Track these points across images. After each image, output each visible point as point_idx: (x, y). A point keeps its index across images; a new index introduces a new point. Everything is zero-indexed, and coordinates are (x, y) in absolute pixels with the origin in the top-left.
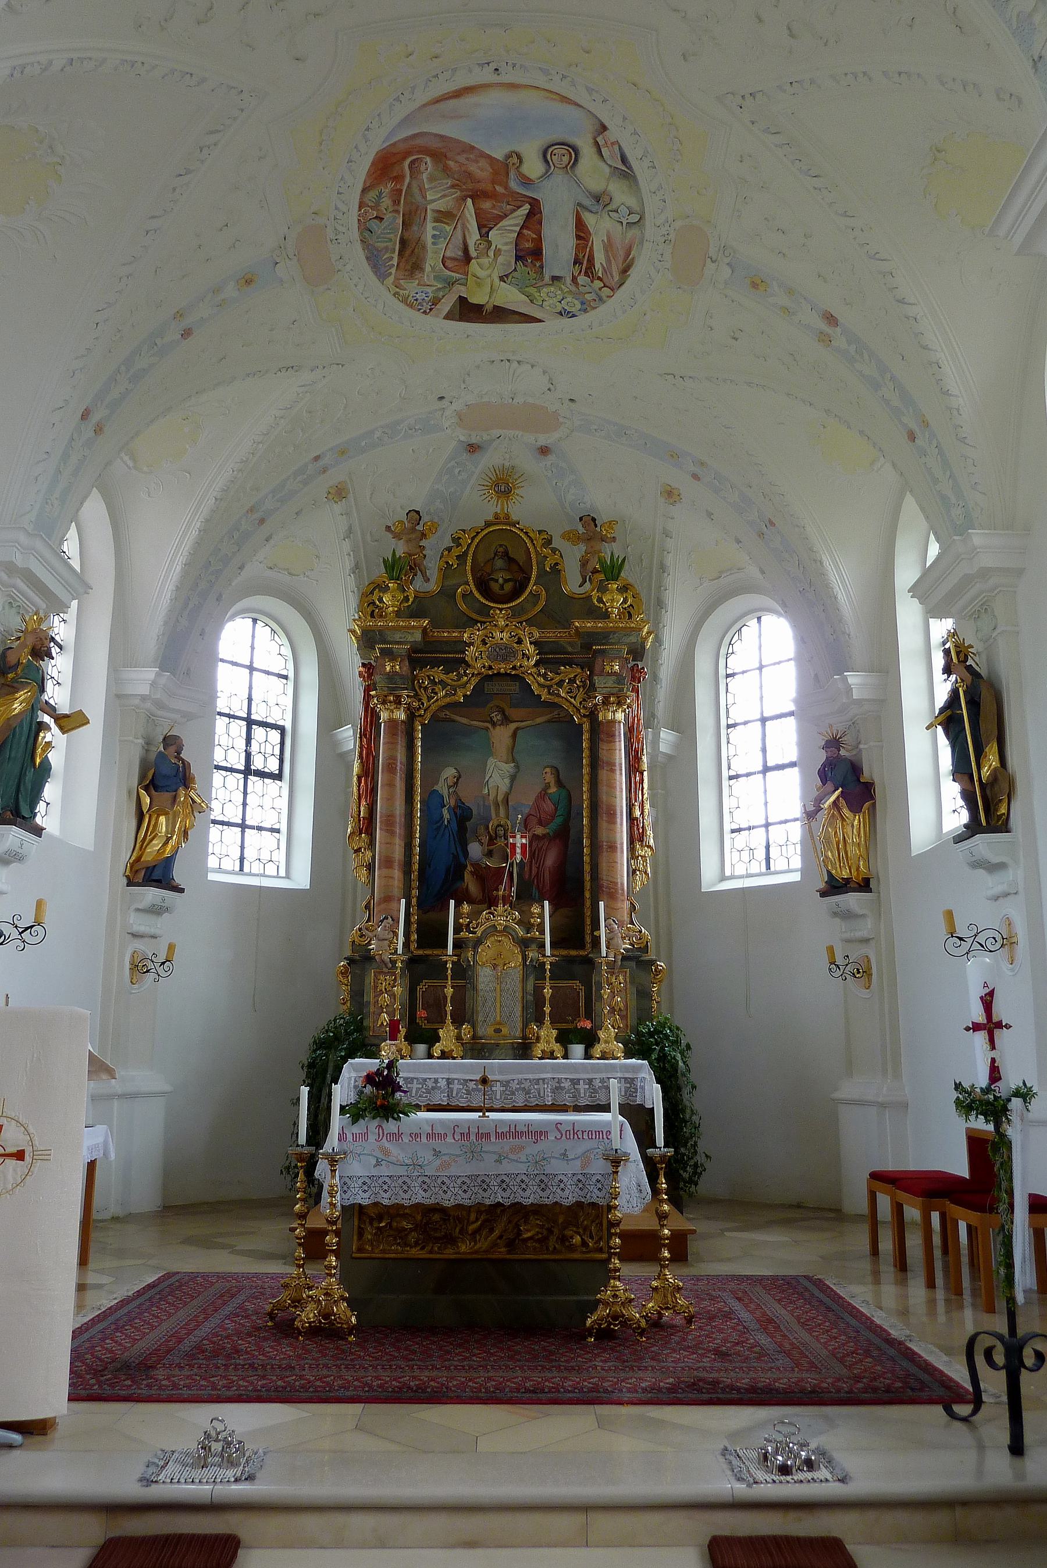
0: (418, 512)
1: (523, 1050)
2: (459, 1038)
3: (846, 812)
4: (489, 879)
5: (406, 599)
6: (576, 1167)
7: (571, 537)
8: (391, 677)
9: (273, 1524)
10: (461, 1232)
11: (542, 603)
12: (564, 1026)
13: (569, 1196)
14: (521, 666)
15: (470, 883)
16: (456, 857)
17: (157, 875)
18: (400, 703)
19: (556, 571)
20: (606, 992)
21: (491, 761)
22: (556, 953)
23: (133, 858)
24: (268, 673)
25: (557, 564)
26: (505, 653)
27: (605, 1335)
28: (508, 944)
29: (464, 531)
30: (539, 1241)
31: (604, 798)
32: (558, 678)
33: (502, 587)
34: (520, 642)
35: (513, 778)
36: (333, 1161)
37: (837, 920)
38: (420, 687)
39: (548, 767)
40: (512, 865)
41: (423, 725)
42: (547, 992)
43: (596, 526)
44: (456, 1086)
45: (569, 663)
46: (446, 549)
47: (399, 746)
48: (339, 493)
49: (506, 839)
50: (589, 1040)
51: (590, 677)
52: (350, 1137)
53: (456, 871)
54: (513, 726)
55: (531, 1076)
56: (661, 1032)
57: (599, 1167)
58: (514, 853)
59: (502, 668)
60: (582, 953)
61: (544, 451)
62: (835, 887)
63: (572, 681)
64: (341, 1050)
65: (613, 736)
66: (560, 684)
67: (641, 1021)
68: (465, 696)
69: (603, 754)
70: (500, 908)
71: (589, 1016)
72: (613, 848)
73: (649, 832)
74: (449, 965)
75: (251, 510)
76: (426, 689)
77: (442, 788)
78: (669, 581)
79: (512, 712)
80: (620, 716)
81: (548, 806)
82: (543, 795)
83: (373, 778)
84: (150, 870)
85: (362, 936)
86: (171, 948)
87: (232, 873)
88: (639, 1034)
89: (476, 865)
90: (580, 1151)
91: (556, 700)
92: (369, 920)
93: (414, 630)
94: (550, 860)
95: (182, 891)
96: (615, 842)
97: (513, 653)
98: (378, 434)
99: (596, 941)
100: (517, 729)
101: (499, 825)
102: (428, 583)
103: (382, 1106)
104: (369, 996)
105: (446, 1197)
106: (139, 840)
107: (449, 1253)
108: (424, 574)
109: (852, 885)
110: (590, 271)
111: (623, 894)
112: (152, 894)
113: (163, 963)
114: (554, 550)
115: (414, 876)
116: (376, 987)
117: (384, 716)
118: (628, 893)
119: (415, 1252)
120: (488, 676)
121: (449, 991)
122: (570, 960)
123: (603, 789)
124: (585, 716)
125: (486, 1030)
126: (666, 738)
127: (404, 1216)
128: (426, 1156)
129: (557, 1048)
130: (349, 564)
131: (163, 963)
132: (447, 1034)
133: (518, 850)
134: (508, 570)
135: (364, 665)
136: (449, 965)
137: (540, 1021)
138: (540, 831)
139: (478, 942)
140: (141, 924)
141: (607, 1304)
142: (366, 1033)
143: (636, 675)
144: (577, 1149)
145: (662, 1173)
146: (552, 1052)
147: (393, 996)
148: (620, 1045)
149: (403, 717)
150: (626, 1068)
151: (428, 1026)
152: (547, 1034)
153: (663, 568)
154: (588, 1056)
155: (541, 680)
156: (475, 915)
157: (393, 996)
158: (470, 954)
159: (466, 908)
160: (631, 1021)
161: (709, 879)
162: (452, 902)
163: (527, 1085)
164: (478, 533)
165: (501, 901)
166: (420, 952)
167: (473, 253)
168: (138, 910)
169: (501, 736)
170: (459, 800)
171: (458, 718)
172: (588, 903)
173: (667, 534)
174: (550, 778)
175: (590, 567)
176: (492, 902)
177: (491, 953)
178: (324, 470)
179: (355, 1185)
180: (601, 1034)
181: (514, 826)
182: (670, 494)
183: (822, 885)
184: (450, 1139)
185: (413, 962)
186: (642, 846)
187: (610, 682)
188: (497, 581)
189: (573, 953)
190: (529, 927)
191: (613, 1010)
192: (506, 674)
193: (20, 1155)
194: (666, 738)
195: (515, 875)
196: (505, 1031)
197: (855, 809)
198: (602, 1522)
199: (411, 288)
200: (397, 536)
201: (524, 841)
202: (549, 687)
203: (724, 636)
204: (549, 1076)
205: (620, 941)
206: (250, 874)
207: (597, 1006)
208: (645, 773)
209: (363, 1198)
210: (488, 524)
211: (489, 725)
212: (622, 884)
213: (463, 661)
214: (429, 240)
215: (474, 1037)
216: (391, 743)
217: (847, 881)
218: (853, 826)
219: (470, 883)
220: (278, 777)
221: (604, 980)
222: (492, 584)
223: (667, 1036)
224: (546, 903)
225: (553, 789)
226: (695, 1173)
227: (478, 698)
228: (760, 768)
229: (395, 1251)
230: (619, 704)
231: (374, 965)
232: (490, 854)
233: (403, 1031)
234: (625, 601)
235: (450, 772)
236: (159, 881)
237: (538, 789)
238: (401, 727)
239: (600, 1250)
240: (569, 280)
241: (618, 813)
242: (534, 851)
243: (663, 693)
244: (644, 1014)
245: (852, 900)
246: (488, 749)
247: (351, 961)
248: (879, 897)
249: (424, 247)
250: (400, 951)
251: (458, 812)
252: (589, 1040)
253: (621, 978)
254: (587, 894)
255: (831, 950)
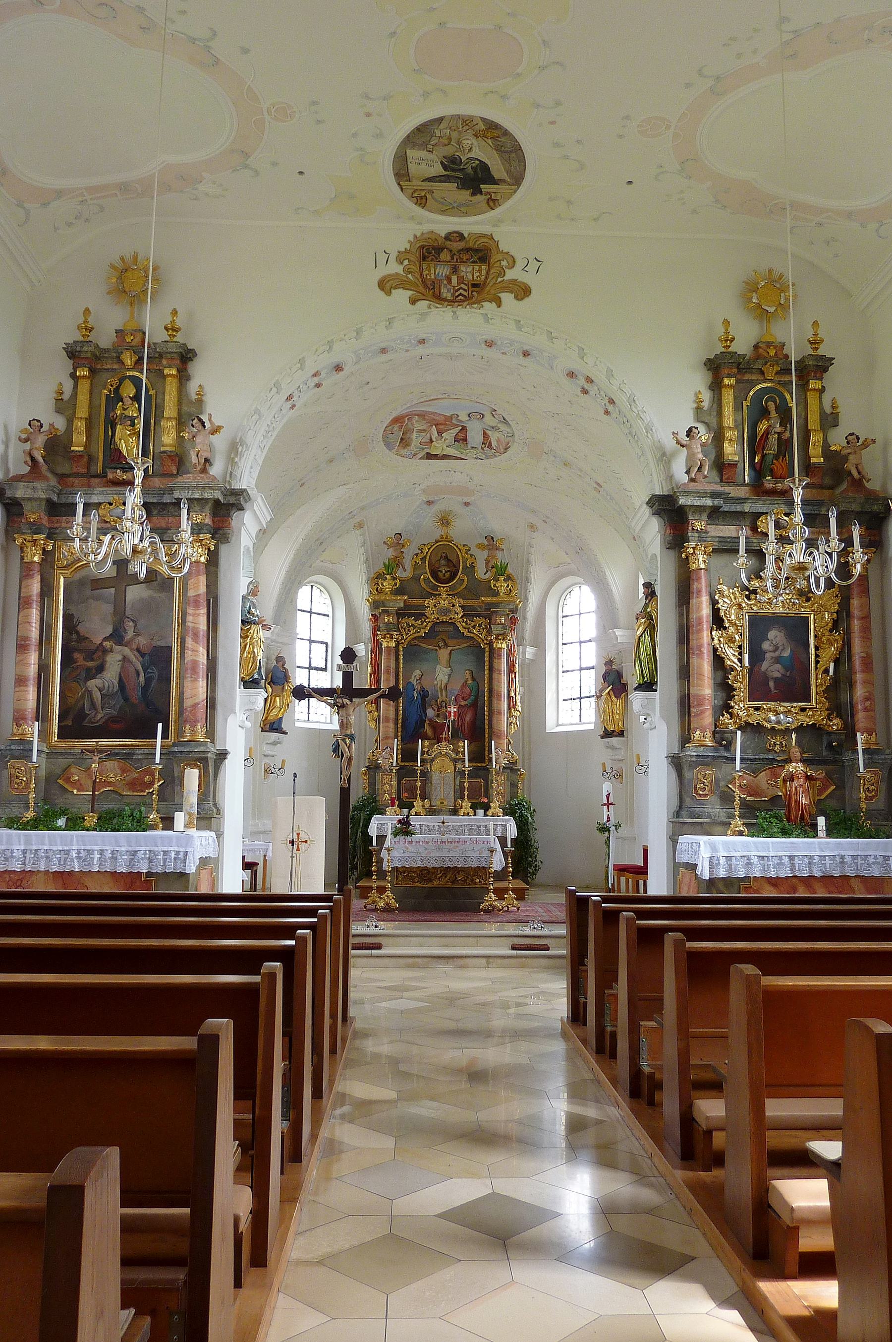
0: (400, 534)
1: (455, 812)
2: (423, 806)
3: (613, 697)
4: (437, 731)
5: (396, 584)
6: (477, 854)
7: (480, 546)
8: (388, 624)
9: (391, 940)
10: (434, 877)
11: (465, 583)
12: (474, 801)
13: (475, 864)
14: (454, 618)
15: (428, 729)
16: (420, 716)
17: (275, 726)
18: (392, 638)
19: (472, 566)
20: (495, 785)
21: (438, 666)
22: (470, 765)
23: (264, 718)
24: (319, 614)
25: (473, 563)
26: (446, 611)
27: (487, 911)
28: (447, 760)
29: (424, 545)
30: (463, 881)
31: (495, 687)
32: (473, 624)
33: (444, 576)
34: (453, 606)
35: (450, 676)
36: (388, 850)
37: (609, 750)
38: (402, 628)
39: (469, 670)
40: (449, 721)
41: (403, 648)
42: (467, 785)
43: (494, 541)
44: (424, 828)
45: (479, 616)
46: (415, 554)
47: (392, 660)
48: (360, 525)
49: (446, 708)
50: (486, 807)
51: (490, 624)
52: (393, 842)
53: (421, 723)
54: (450, 648)
55: (458, 824)
56: (521, 804)
57: (486, 853)
58: (450, 715)
59: (445, 619)
60: (484, 765)
61: (467, 504)
62: (607, 734)
63: (480, 625)
64: (367, 811)
65: (501, 656)
66: (474, 627)
67: (512, 798)
68: (425, 633)
69: (495, 665)
70: (443, 743)
71: (487, 796)
72: (499, 713)
73: (519, 704)
74: (419, 772)
75: (317, 540)
76: (404, 629)
77: (413, 681)
78: (532, 569)
79: (450, 642)
80: (504, 646)
81: (467, 690)
82: (465, 684)
83: (378, 675)
84: (272, 724)
85: (373, 756)
86: (283, 761)
87: (304, 721)
88: (510, 805)
89: (430, 720)
90: (479, 848)
91: (472, 635)
92: (376, 749)
93: (399, 602)
94: (468, 718)
95: (287, 733)
96: (501, 710)
97: (450, 612)
98: (382, 500)
99: (490, 760)
100: (452, 650)
101: (443, 701)
102: (405, 573)
103: (405, 831)
104: (379, 786)
105: (430, 864)
106: (266, 709)
107: (430, 885)
108: (403, 568)
109: (615, 734)
110: (490, 446)
111: (504, 736)
112: (274, 736)
113: (280, 769)
114: (471, 555)
115: (400, 726)
116: (382, 781)
117: (384, 645)
118: (507, 735)
119: (418, 885)
120: (437, 622)
121: (419, 784)
122: (477, 768)
123: (495, 683)
124: (486, 644)
125: (436, 803)
126: (530, 652)
127: (413, 872)
128: (422, 850)
129: (471, 811)
130: (363, 558)
131: (280, 769)
132: (418, 804)
133: (452, 714)
134: (448, 566)
135: (372, 615)
136: (419, 772)
137: (462, 798)
138: (463, 703)
139: (433, 760)
140: (267, 750)
141: (487, 901)
142: (378, 803)
143: (513, 621)
144: (477, 847)
145: (509, 857)
146: (468, 813)
147: (391, 785)
148: (501, 810)
149: (394, 645)
150: (503, 820)
151: (408, 800)
152: (466, 805)
153: (529, 562)
154: (485, 815)
155: (464, 624)
156: (431, 746)
157: (391, 785)
158: (428, 766)
159: (426, 743)
160: (507, 798)
161: (551, 726)
162: (420, 740)
163: (456, 828)
164: (432, 546)
165: (444, 740)
166: (403, 764)
167: (434, 439)
168: (267, 743)
169: (444, 654)
170: (422, 687)
171: (421, 644)
172: (487, 740)
173: (530, 545)
174: (468, 676)
175: (490, 565)
176: (439, 741)
177: (439, 765)
178: (354, 516)
179: (396, 860)
180: (492, 805)
181: (450, 701)
182: (532, 527)
183: (602, 733)
184: (430, 843)
185: (401, 769)
186: (515, 710)
187: (500, 628)
188: (441, 572)
189: (479, 765)
190: (457, 753)
191: (498, 794)
192: (446, 622)
193: (306, 842)
194: (530, 652)
195: (450, 726)
196: (445, 803)
197: (618, 697)
198: (481, 940)
199: (404, 452)
200: (389, 547)
201: (455, 710)
202: (469, 628)
203: (562, 595)
204: (467, 823)
205: (502, 760)
206: (313, 722)
207: (490, 791)
208: (517, 674)
209: (399, 865)
210: (437, 542)
211: (438, 648)
212: (504, 731)
213: (424, 614)
214: (414, 437)
215: (430, 806)
216: (388, 659)
217: (613, 731)
218: (616, 704)
219: (428, 729)
220: (325, 670)
221: (494, 779)
222: (439, 573)
223: (524, 805)
224: (466, 741)
225: (470, 682)
226: (535, 870)
227: (432, 634)
228: (579, 668)
229: (410, 884)
230: (504, 639)
231: (381, 770)
232: (438, 716)
233: (397, 803)
234: (508, 586)
235: (417, 673)
236: (277, 729)
237: (463, 681)
238: (393, 651)
239: (486, 884)
240: (480, 448)
241: (503, 695)
242: (460, 715)
243: (529, 626)
244: (514, 795)
245: (614, 740)
246: (437, 661)
247: (368, 768)
248: (628, 740)
249: (412, 440)
250: (394, 765)
251: (422, 693)
252: (486, 807)
253: (502, 778)
254: (487, 736)
255: (604, 765)
